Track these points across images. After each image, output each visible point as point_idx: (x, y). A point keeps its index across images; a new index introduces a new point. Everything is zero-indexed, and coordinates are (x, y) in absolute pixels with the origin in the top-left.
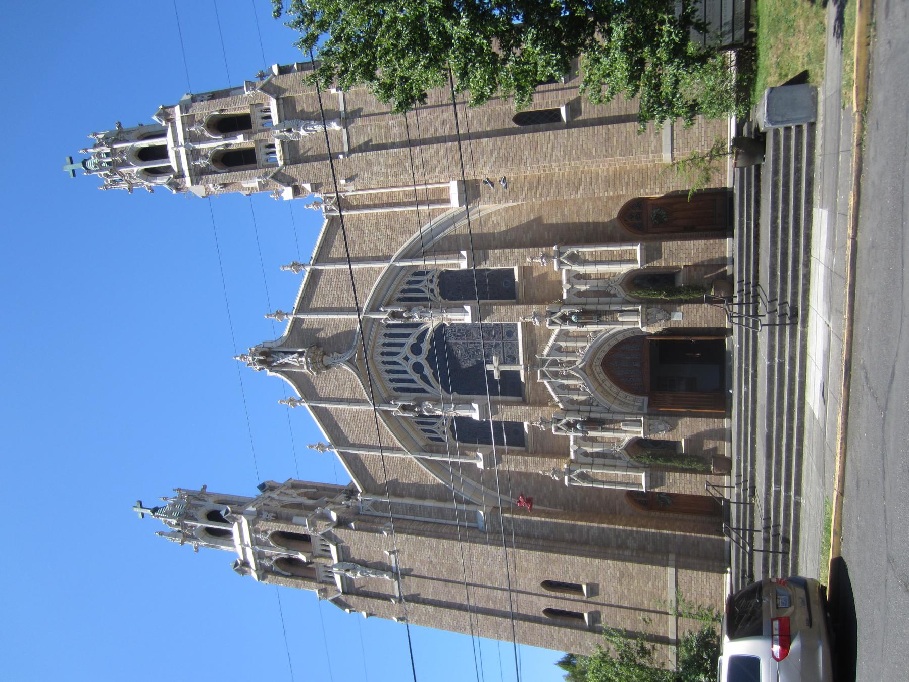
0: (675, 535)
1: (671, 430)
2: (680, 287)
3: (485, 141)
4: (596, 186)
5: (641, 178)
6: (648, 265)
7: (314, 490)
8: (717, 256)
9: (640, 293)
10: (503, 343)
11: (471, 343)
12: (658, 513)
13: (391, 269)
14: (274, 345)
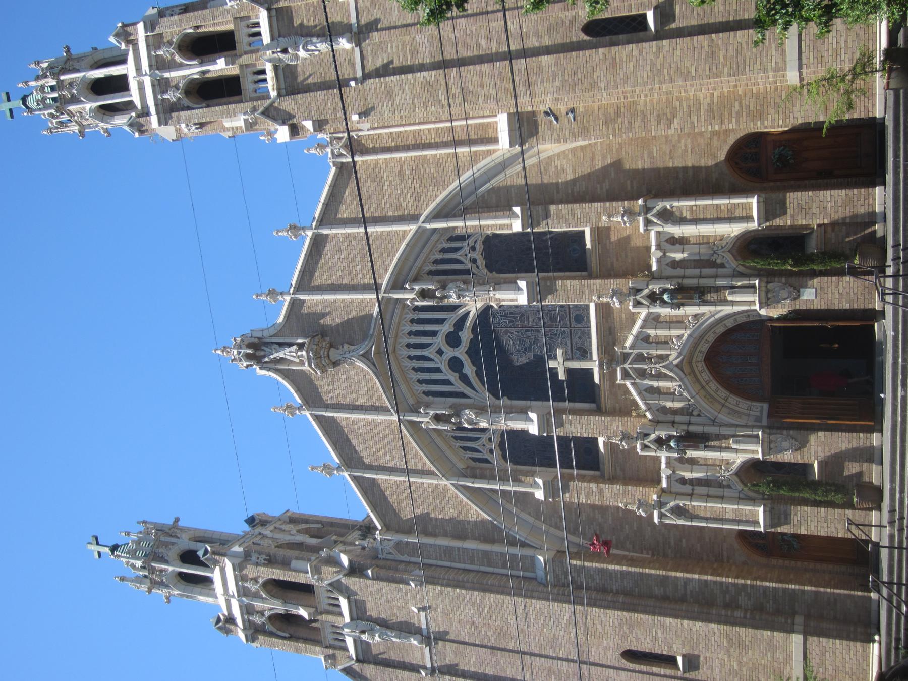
0: (803, 591)
1: (799, 449)
2: (813, 254)
3: (544, 59)
4: (696, 117)
5: (758, 105)
6: (768, 224)
7: (320, 526)
8: (863, 211)
9: (758, 263)
10: (571, 330)
11: (527, 331)
12: (781, 561)
13: (420, 232)
14: (266, 334)
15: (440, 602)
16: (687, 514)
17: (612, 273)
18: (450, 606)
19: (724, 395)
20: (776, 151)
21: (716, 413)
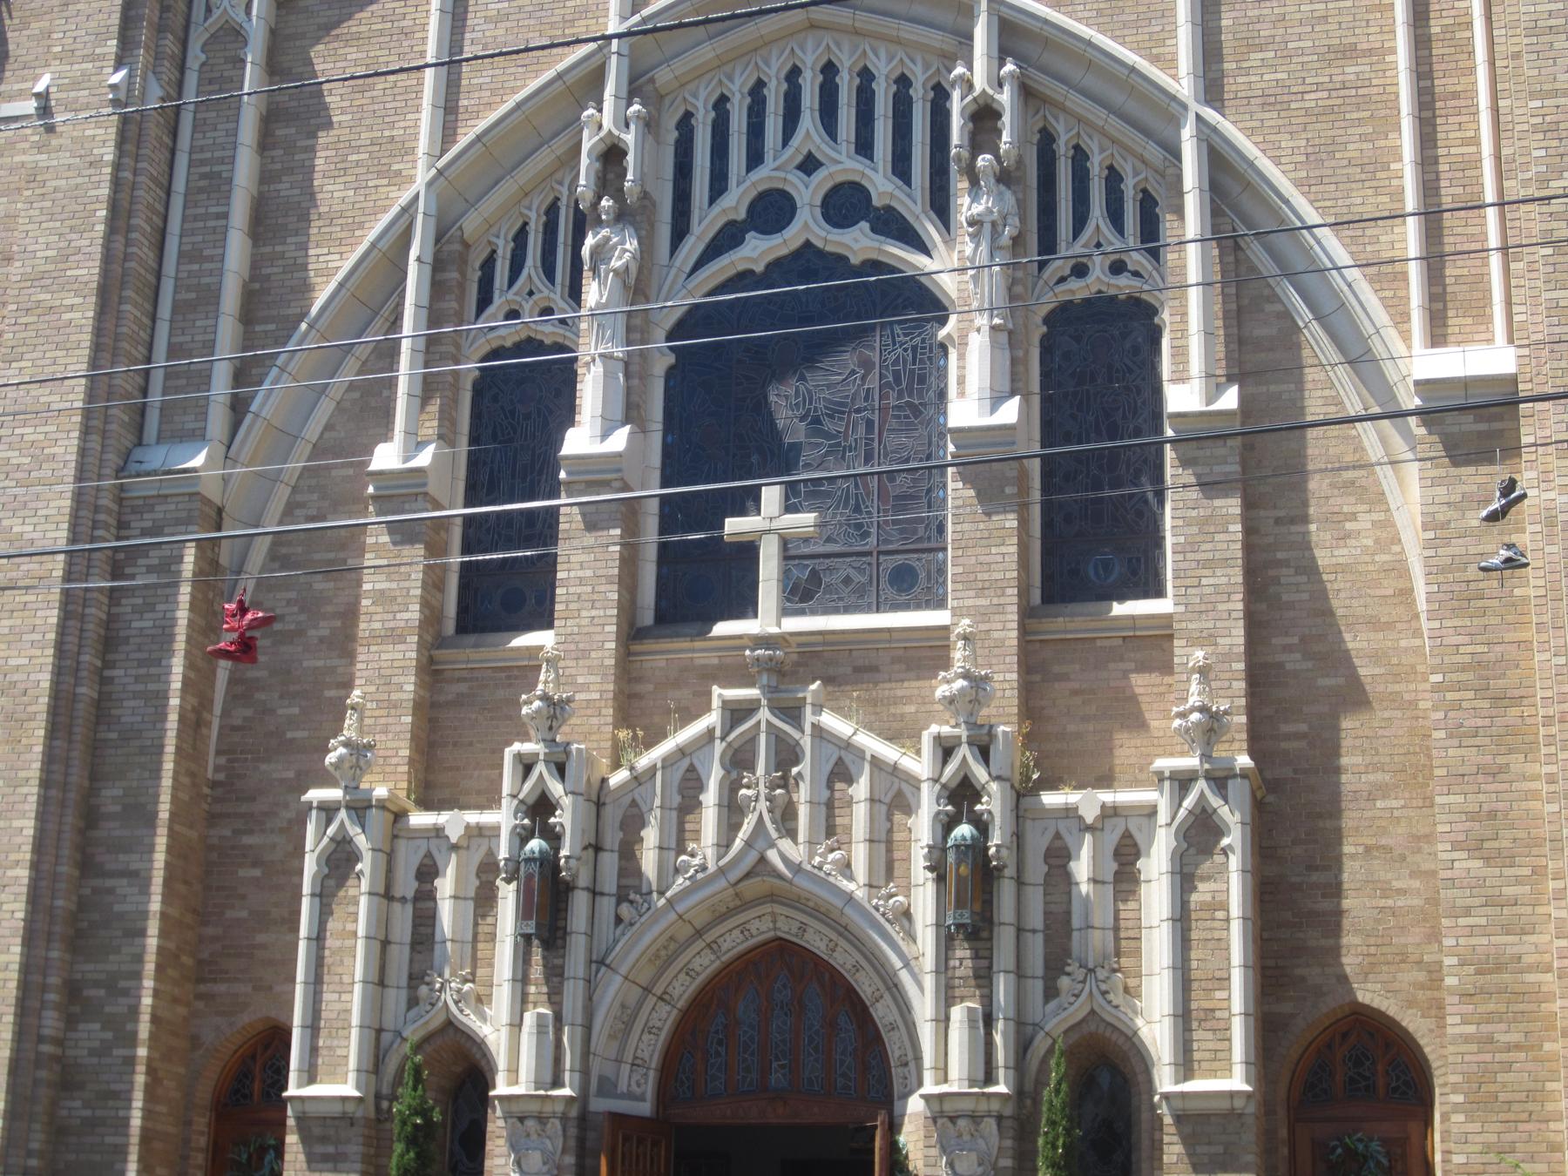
4: (1483, 921)
6: (1168, 1120)
9: (1057, 1091)
10: (869, 554)
11: (869, 424)
12: (203, 1141)
13: (1170, 109)
15: (65, 158)
16: (332, 882)
17: (1037, 678)
18: (56, 190)
19: (676, 993)
20: (1375, 1146)
21: (623, 970)
